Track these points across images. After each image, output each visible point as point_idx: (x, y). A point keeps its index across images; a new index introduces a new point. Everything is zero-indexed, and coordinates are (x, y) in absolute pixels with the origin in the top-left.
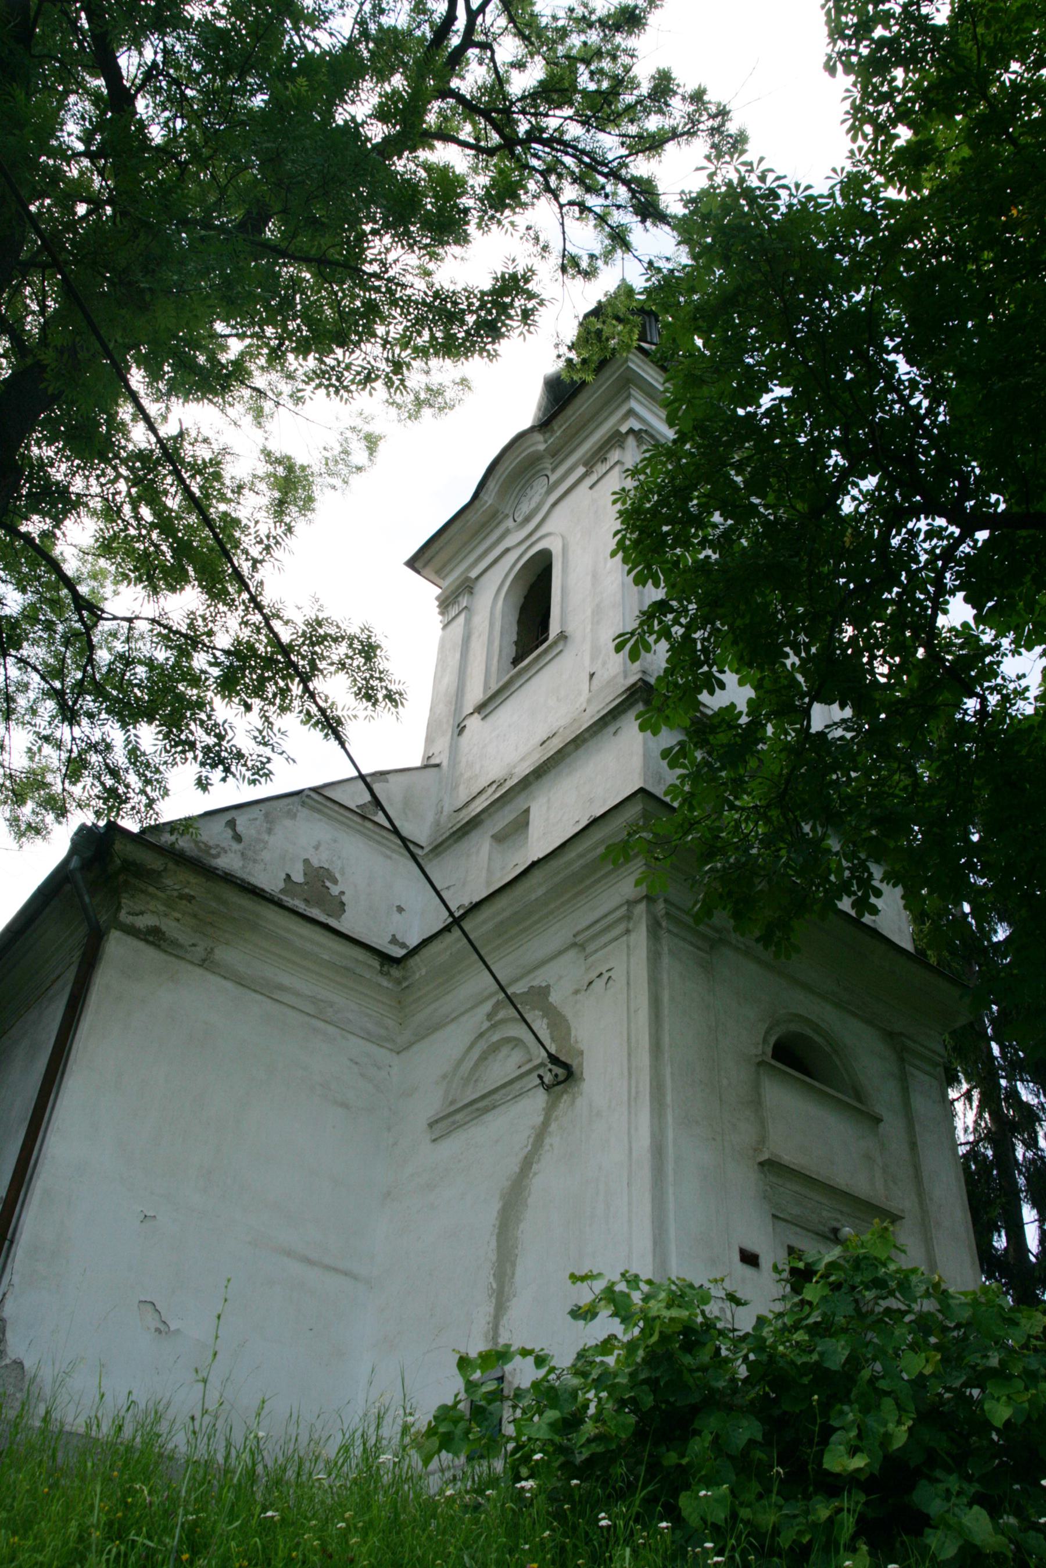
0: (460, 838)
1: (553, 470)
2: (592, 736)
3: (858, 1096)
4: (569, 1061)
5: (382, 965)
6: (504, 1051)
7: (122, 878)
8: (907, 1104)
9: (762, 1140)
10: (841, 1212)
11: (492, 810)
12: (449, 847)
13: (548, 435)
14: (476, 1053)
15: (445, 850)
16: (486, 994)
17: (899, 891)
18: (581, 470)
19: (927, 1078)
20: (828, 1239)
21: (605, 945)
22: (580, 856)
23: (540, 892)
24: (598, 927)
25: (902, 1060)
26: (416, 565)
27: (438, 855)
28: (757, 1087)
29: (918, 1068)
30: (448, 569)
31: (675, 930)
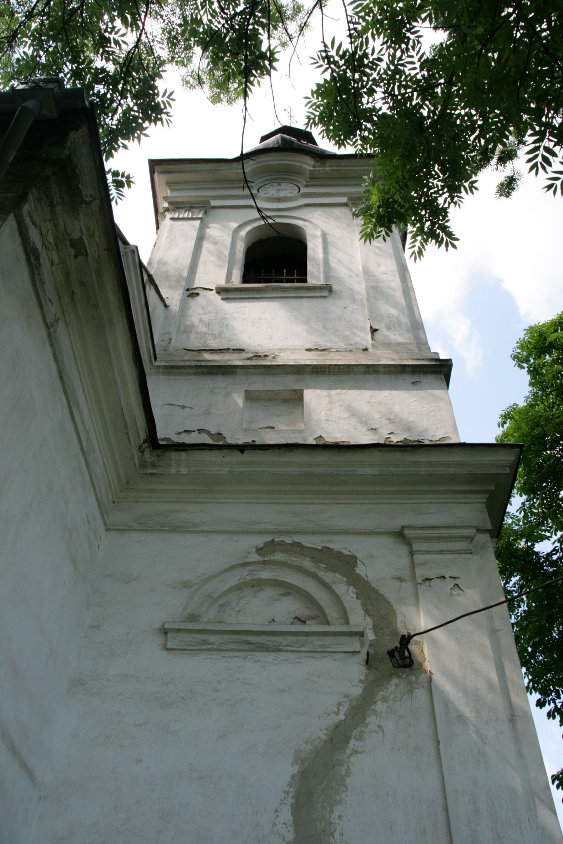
0: (203, 374)
1: (306, 186)
2: (385, 373)
5: (145, 441)
6: (268, 593)
7: (48, 171)
11: (252, 371)
12: (188, 374)
13: (319, 164)
14: (233, 579)
15: (180, 374)
16: (258, 527)
18: (344, 200)
21: (442, 552)
22: (430, 464)
23: (370, 471)
24: (435, 533)
26: (156, 167)
27: (168, 374)
30: (181, 187)
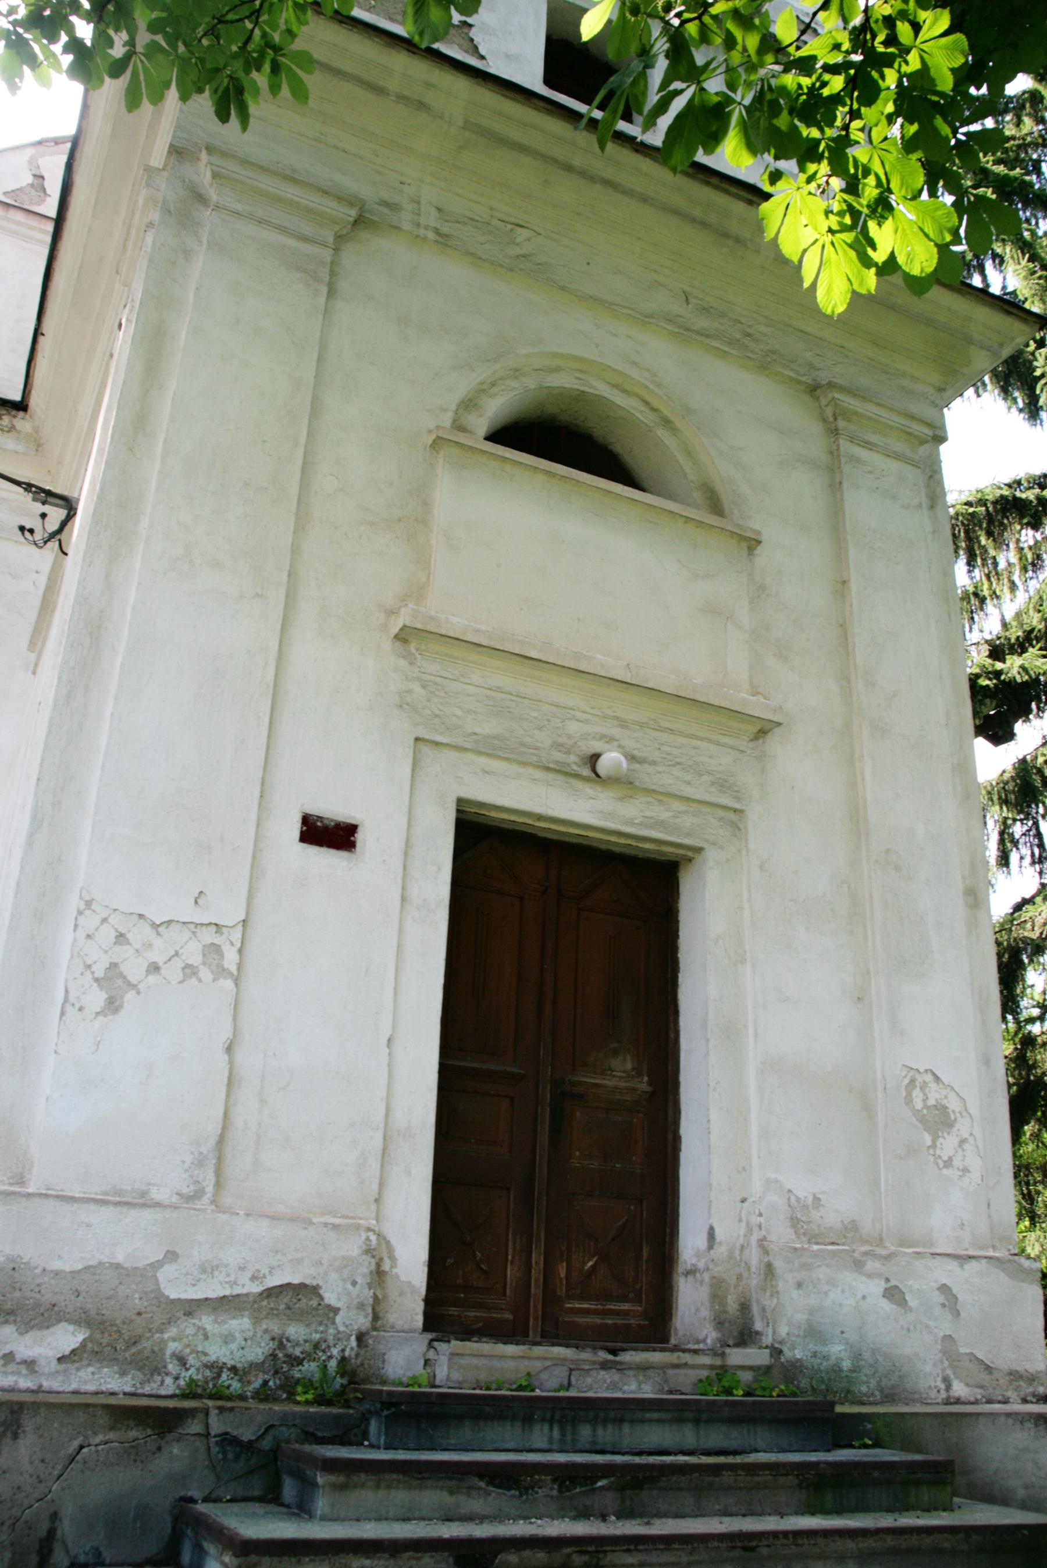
3: (715, 505)
4: (65, 493)
8: (836, 512)
9: (417, 592)
10: (623, 724)
17: (848, 151)
19: (894, 466)
20: (577, 776)
25: (834, 432)
28: (421, 494)
29: (867, 445)
31: (239, 207)
